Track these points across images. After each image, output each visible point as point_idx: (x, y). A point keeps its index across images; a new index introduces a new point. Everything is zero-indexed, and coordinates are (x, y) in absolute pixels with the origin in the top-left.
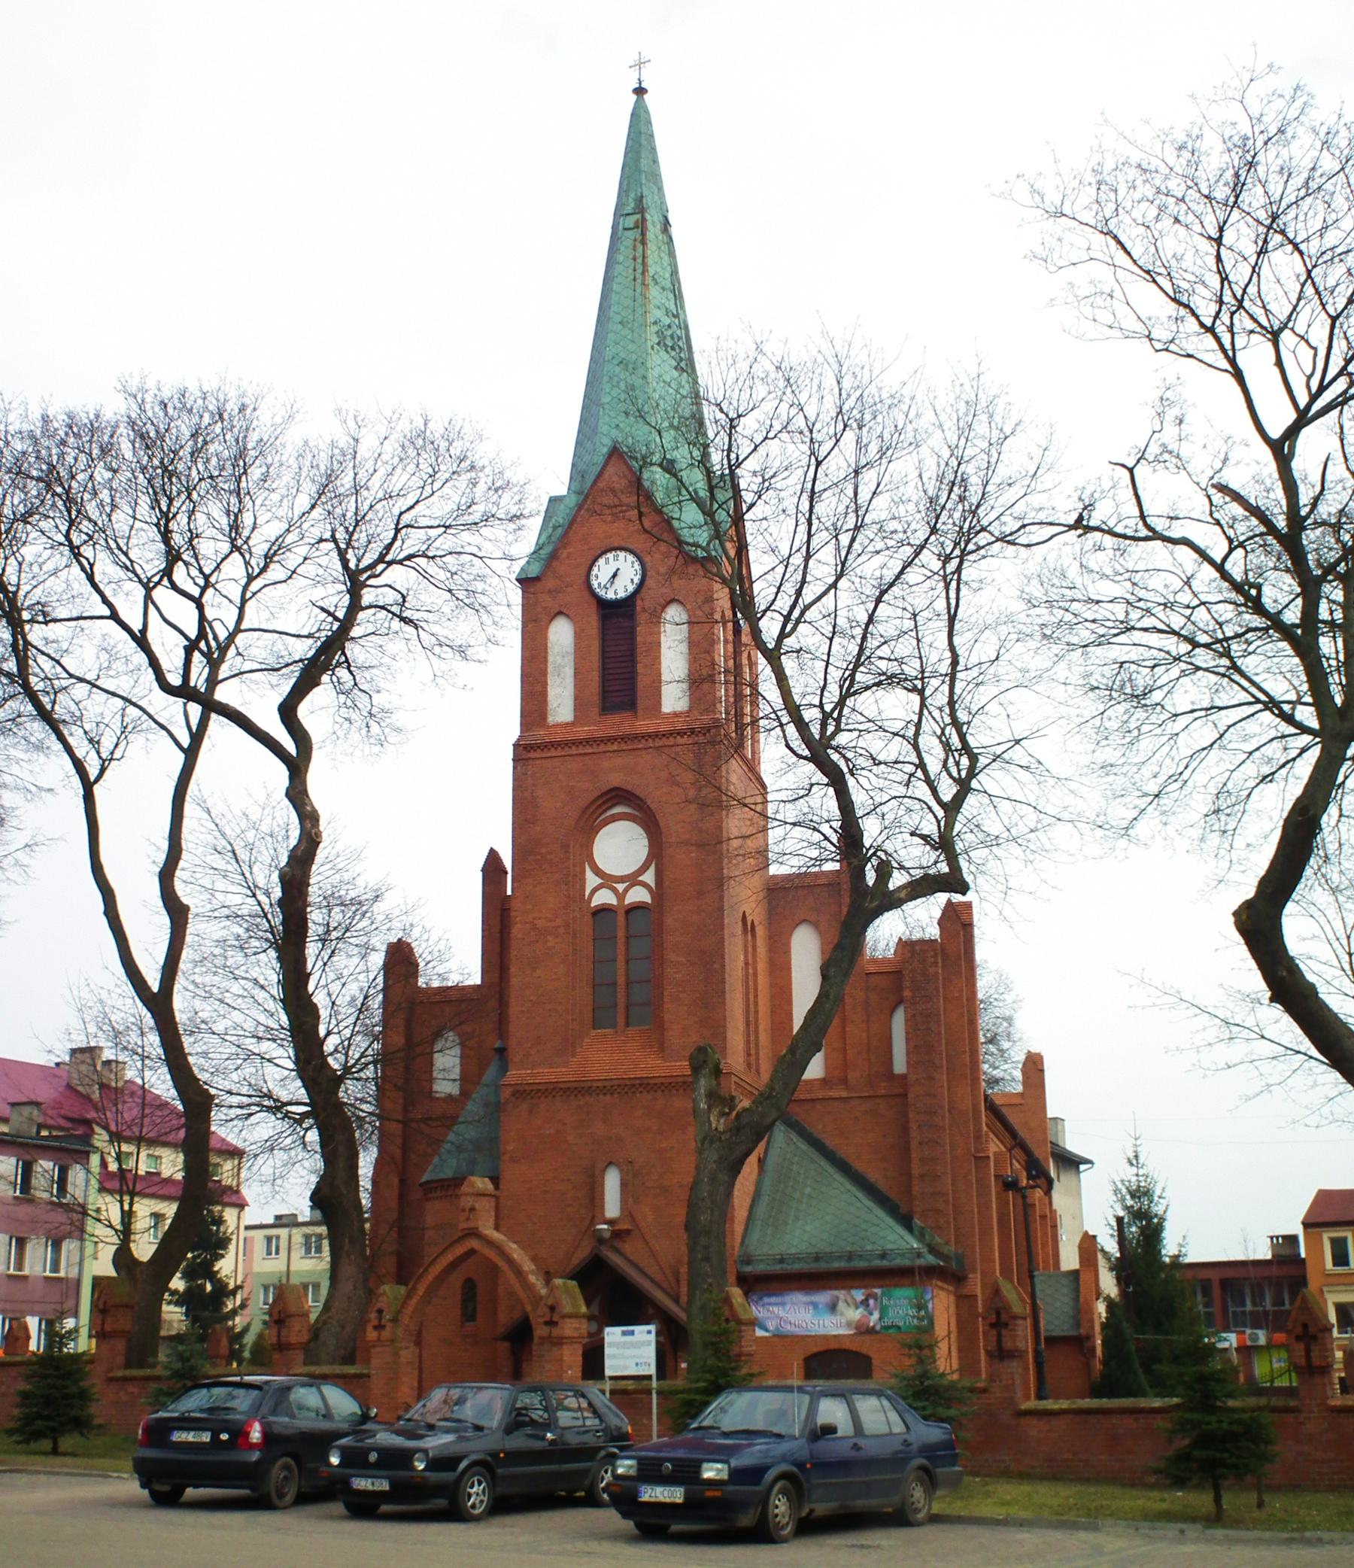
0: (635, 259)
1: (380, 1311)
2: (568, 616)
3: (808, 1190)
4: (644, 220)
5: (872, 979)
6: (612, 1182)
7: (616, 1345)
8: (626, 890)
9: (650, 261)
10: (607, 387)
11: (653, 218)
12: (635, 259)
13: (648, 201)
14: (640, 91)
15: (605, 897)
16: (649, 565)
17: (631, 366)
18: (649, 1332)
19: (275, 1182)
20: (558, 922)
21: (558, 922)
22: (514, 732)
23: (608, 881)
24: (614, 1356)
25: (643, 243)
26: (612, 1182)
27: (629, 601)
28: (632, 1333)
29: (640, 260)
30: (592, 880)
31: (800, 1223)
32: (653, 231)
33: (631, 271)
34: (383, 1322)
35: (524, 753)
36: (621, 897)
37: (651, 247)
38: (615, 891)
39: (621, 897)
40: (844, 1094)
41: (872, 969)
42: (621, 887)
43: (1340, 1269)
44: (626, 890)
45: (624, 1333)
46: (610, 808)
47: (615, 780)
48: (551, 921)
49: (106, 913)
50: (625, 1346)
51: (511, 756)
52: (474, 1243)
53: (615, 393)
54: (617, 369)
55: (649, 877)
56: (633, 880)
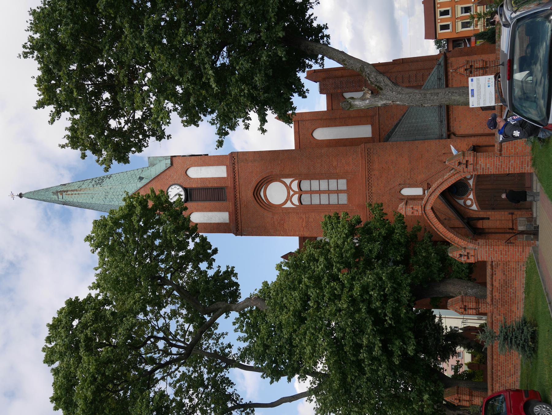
0: (72, 194)
1: (461, 255)
2: (190, 215)
3: (414, 121)
4: (60, 192)
5: (334, 108)
6: (407, 192)
7: (479, 99)
8: (293, 191)
9: (73, 189)
10: (113, 203)
11: (60, 189)
12: (72, 194)
13: (55, 191)
14: (21, 196)
15: (295, 199)
16: (173, 183)
17: (107, 194)
18: (472, 80)
19: (395, 285)
20: (304, 216)
21: (304, 216)
22: (232, 235)
23: (289, 198)
24: (485, 100)
25: (67, 191)
26: (407, 192)
27: (185, 190)
28: (472, 90)
29: (73, 192)
30: (289, 205)
31: (427, 119)
32: (65, 189)
33: (76, 196)
34: (466, 254)
35: (238, 232)
36: (295, 193)
37: (69, 188)
38: (293, 195)
39: (295, 193)
40: (377, 116)
41: (330, 108)
42: (292, 193)
43: (451, 27)
44: (293, 191)
45: (473, 96)
46: (260, 196)
47: (250, 193)
48: (303, 220)
49: (290, 401)
50: (479, 95)
51: (240, 236)
52: (428, 208)
53: (115, 200)
54: (107, 199)
55: (288, 181)
56: (289, 188)
